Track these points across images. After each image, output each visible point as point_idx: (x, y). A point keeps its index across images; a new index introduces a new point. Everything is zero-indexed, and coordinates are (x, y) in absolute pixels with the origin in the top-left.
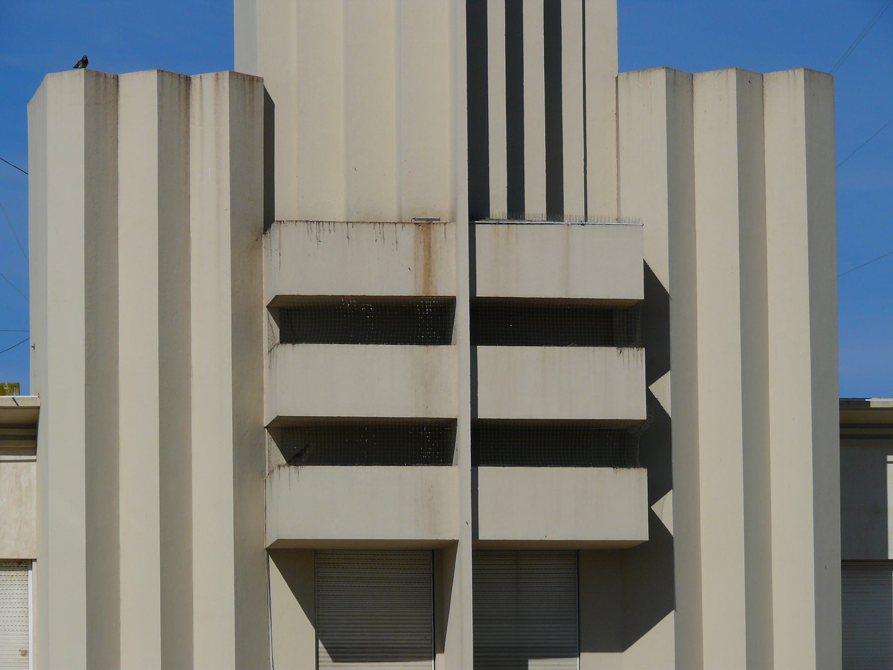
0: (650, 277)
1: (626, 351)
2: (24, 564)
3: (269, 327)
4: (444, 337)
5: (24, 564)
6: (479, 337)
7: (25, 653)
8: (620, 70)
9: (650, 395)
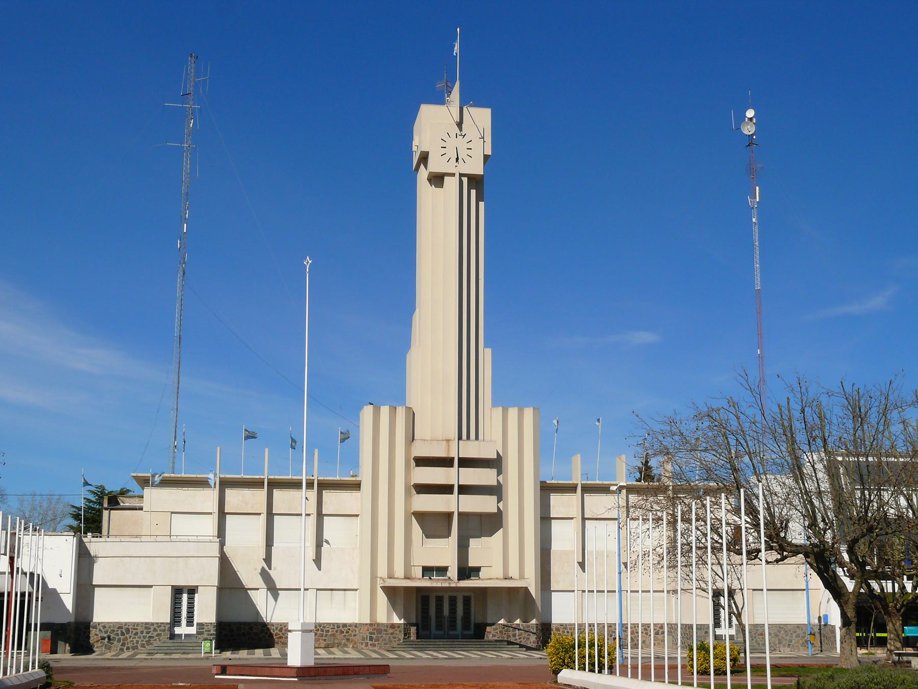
0: (498, 453)
1: (492, 469)
2: (357, 516)
3: (413, 463)
4: (451, 465)
5: (357, 516)
7: (357, 536)
8: (492, 407)
9: (498, 506)
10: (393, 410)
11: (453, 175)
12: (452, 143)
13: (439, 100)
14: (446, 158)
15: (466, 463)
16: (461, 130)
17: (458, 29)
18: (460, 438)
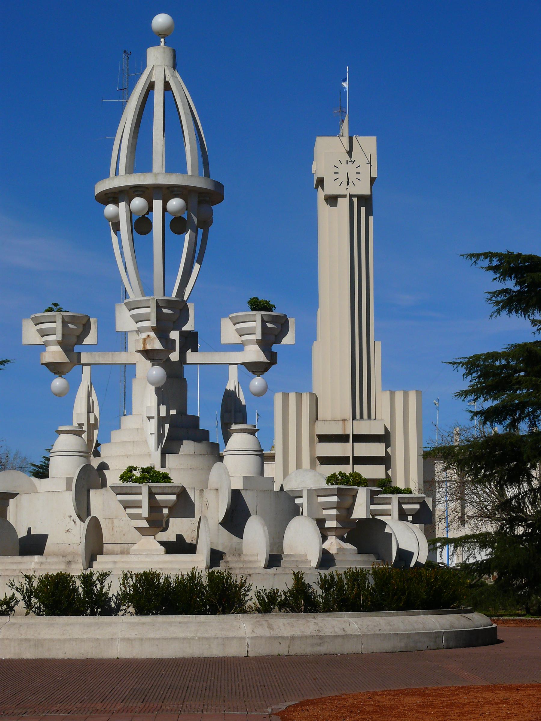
0: (386, 429)
3: (317, 439)
6: (354, 441)
10: (299, 396)
11: (345, 196)
12: (343, 169)
13: (335, 132)
14: (338, 182)
15: (359, 438)
16: (351, 157)
17: (347, 68)
18: (354, 417)
